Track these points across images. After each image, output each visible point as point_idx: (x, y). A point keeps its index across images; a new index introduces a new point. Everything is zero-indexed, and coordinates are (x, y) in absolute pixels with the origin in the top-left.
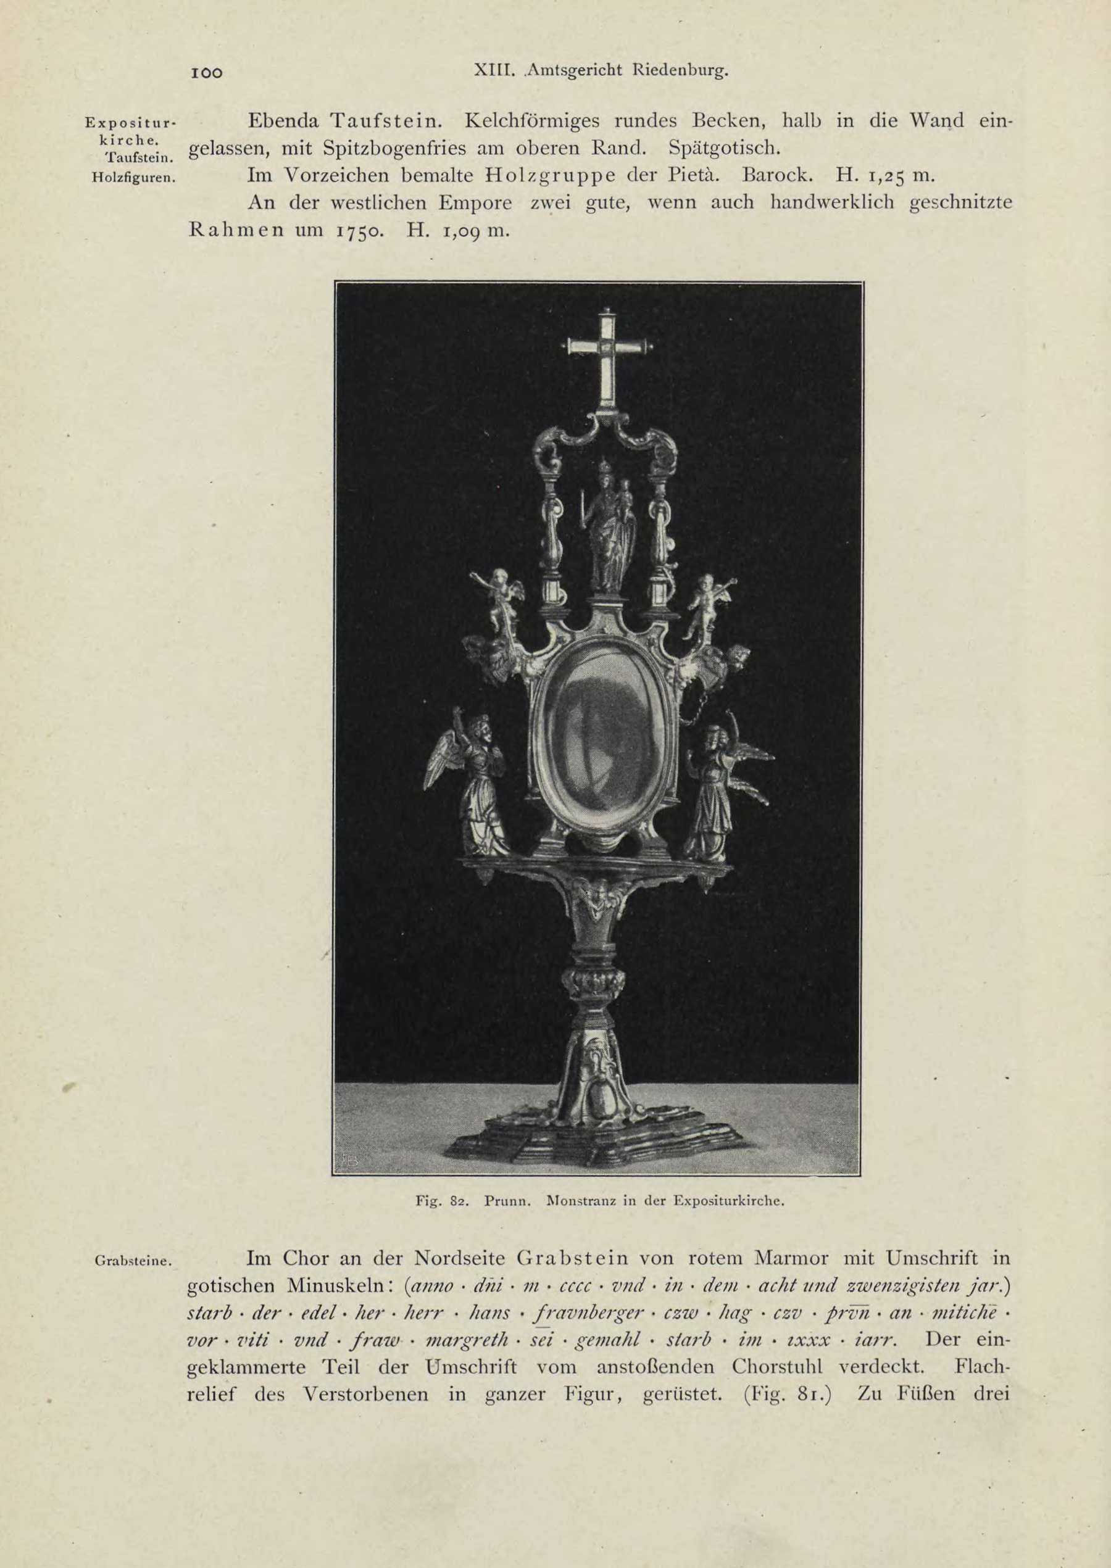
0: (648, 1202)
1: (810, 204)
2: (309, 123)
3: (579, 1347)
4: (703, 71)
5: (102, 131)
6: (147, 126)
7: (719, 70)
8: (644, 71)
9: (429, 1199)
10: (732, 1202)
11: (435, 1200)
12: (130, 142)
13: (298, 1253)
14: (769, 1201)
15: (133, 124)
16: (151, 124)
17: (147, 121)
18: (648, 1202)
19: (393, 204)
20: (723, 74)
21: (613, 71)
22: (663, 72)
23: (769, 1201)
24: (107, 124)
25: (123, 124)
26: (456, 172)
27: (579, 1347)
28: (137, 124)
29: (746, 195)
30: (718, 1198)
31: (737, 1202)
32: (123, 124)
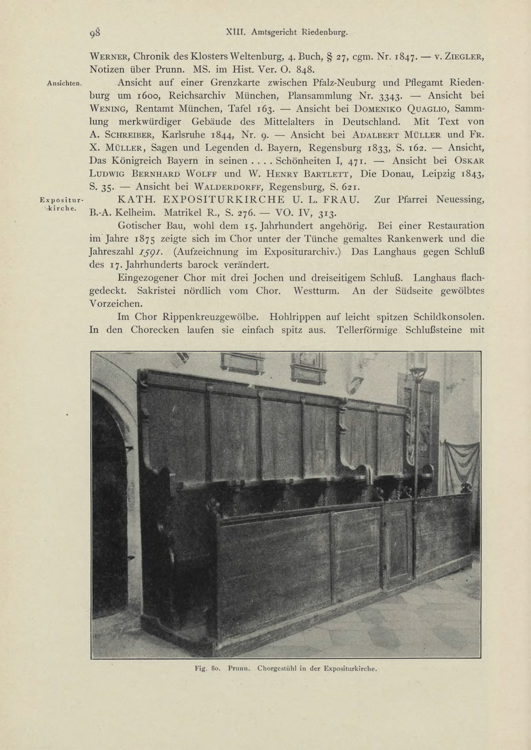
0: (312, 669)
4: (335, 33)
5: (48, 204)
6: (70, 202)
7: (343, 32)
8: (307, 32)
9: (201, 667)
10: (352, 669)
11: (204, 668)
12: (62, 209)
14: (369, 669)
15: (62, 200)
16: (71, 201)
17: (70, 199)
18: (312, 669)
20: (345, 34)
21: (292, 32)
22: (317, 33)
23: (369, 669)
24: (50, 201)
25: (58, 201)
28: (65, 201)
30: (345, 667)
31: (354, 669)
32: (58, 201)
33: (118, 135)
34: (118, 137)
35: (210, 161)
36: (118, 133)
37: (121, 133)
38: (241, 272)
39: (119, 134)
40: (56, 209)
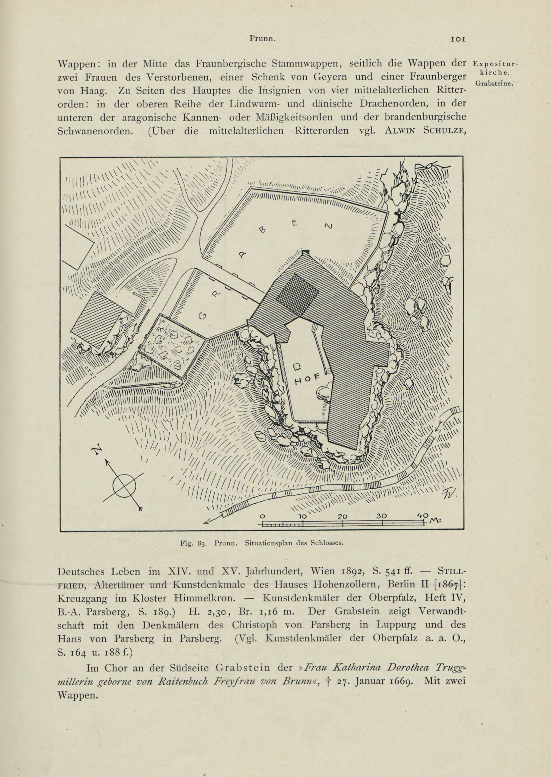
1: (248, 105)
2: (180, 65)
3: (100, 685)
5: (481, 68)
12: (495, 73)
13: (112, 665)
15: (496, 64)
16: (506, 64)
17: (504, 63)
19: (341, 104)
24: (484, 65)
25: (492, 64)
26: (389, 88)
27: (100, 685)
28: (499, 64)
29: (383, 100)
32: (492, 64)
33: (437, 131)
34: (437, 133)
35: (442, 104)
36: (437, 129)
37: (440, 129)
38: (373, 111)
39: (438, 129)
40: (488, 73)
